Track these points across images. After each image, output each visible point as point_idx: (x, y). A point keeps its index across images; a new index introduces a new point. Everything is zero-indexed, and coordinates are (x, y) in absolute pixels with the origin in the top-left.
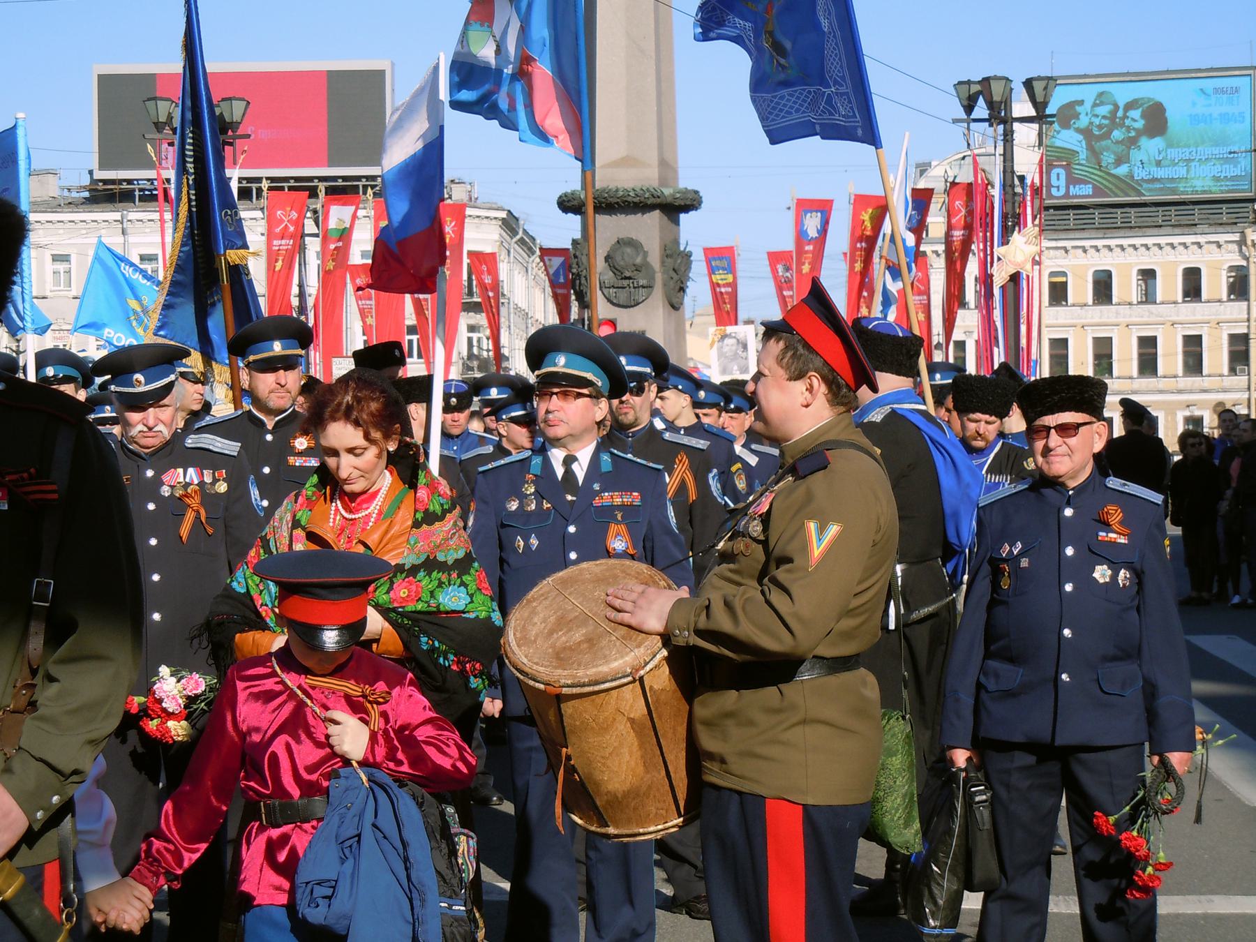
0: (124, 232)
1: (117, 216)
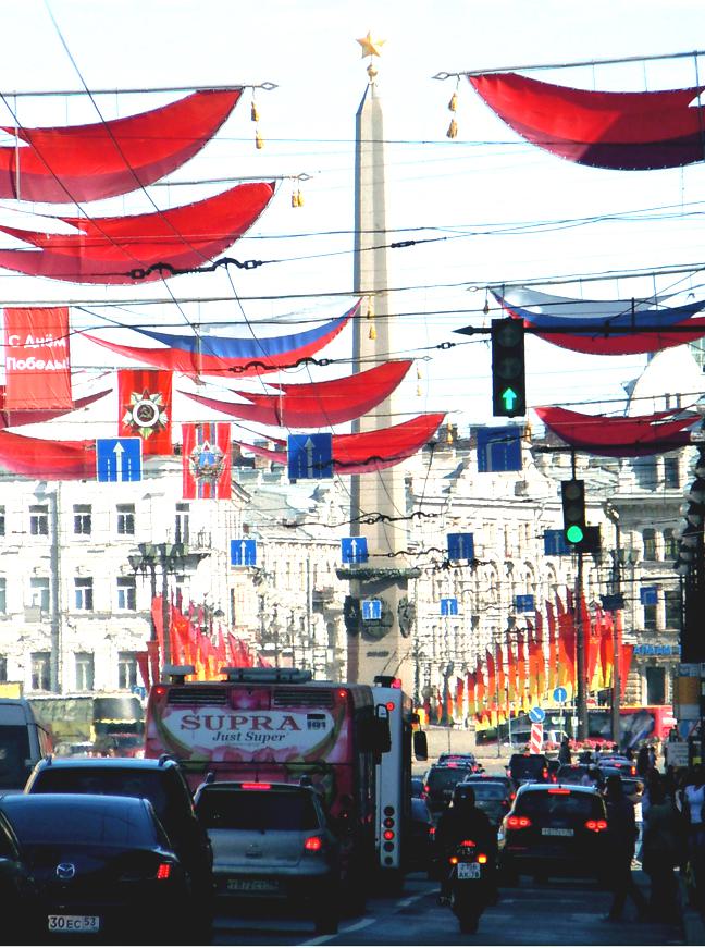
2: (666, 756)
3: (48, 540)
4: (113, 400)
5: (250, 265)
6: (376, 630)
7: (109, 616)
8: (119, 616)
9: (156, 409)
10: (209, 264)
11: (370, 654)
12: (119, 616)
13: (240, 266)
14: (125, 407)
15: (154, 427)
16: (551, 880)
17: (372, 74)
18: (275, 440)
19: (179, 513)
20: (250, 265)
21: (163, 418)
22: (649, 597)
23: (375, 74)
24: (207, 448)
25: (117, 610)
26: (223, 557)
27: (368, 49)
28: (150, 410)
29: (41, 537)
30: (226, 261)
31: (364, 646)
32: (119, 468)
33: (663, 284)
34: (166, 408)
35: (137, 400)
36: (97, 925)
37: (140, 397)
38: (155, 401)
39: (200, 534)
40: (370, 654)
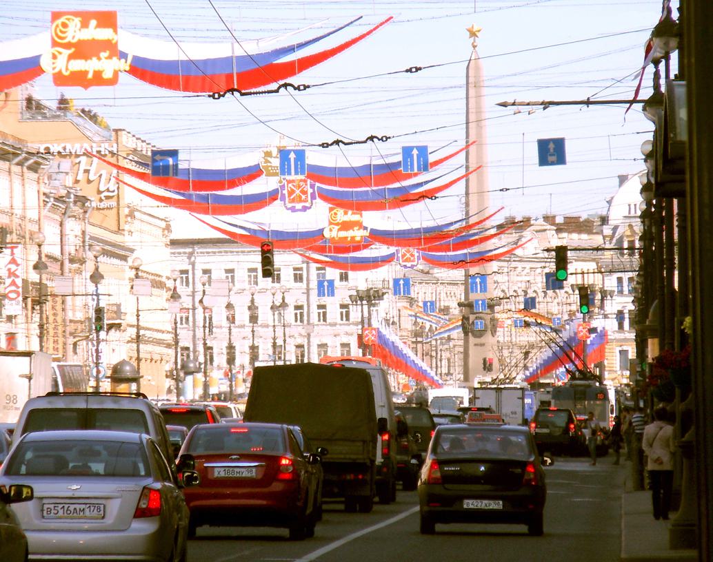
2: (579, 358)
3: (304, 285)
5: (302, 88)
6: (478, 333)
7: (334, 325)
8: (340, 325)
10: (274, 86)
11: (475, 345)
12: (340, 325)
17: (475, 47)
18: (76, 14)
20: (302, 88)
22: (620, 315)
23: (476, 46)
25: (339, 321)
26: (561, 421)
27: (473, 34)
29: (299, 284)
30: (285, 85)
31: (472, 340)
32: (402, 291)
39: (383, 281)
40: (475, 345)
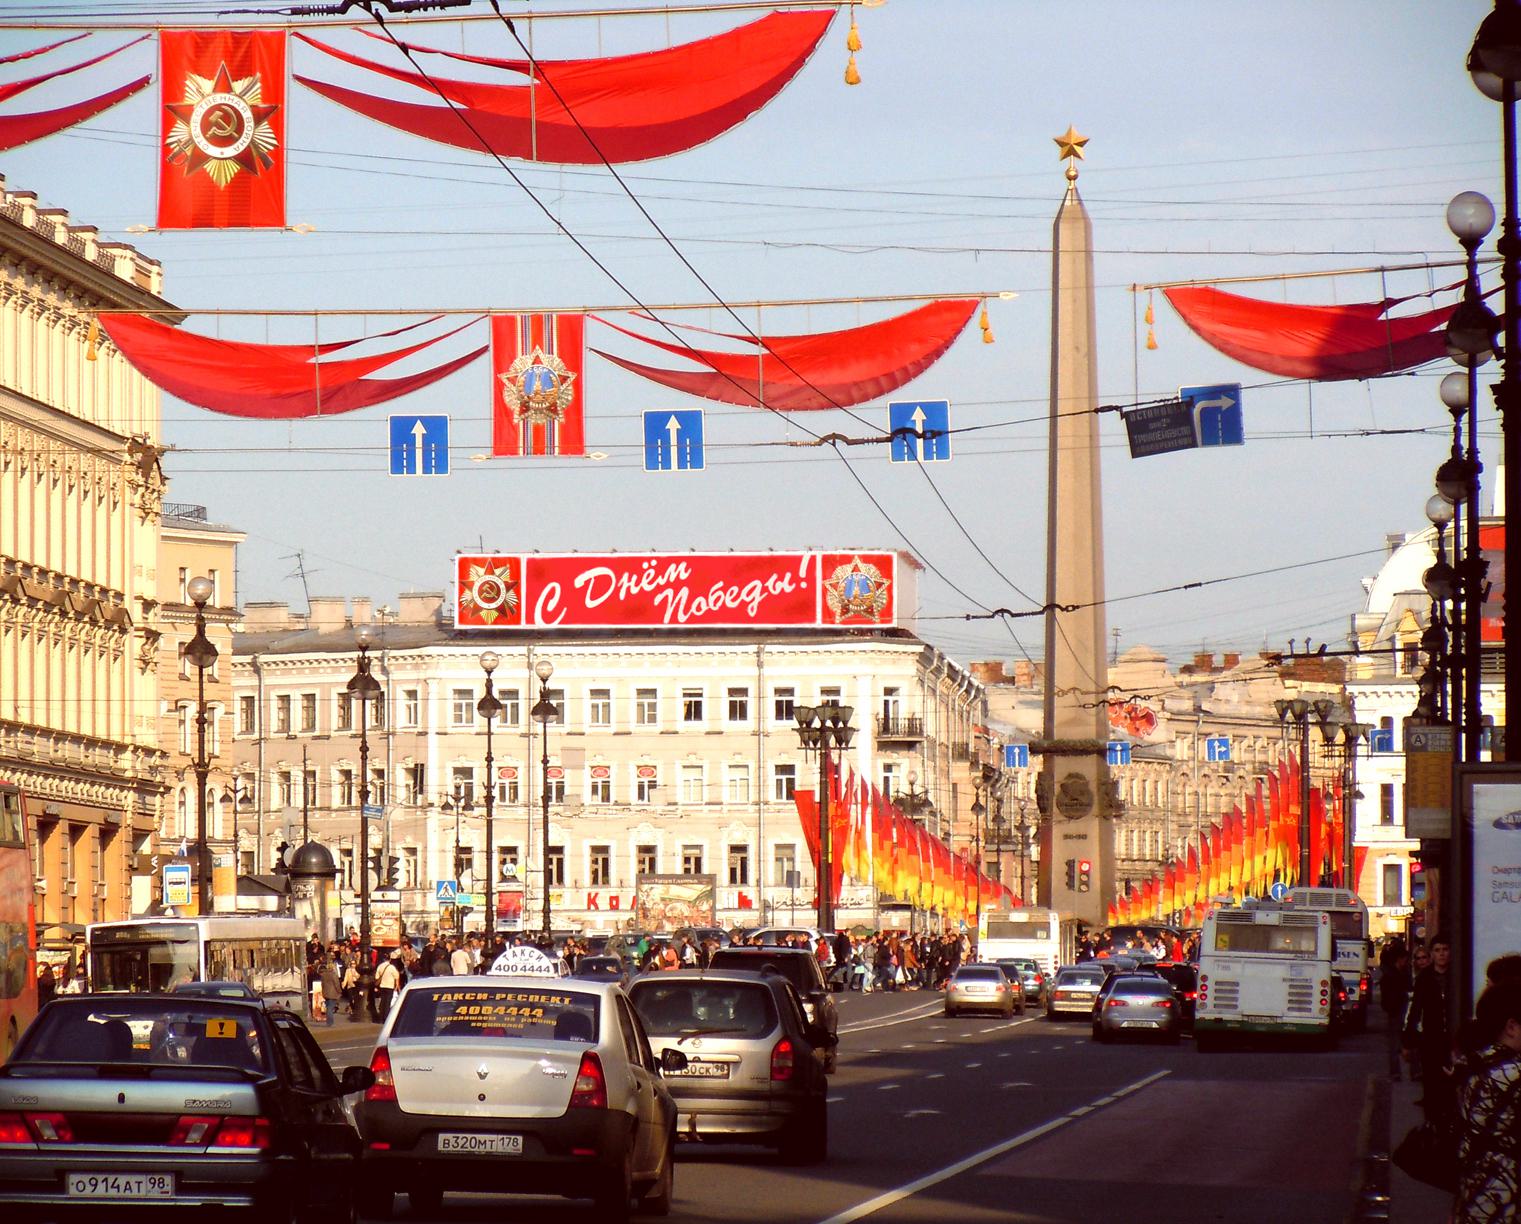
0: (760, 665)
1: (754, 648)
4: (149, 101)
9: (247, 115)
13: (1062, 609)
14: (172, 111)
15: (244, 159)
16: (1439, 705)
19: (887, 698)
21: (264, 135)
24: (537, 361)
27: (1069, 150)
28: (232, 117)
33: (1397, 285)
34: (271, 112)
35: (200, 92)
36: (520, 1146)
37: (207, 85)
38: (245, 95)
